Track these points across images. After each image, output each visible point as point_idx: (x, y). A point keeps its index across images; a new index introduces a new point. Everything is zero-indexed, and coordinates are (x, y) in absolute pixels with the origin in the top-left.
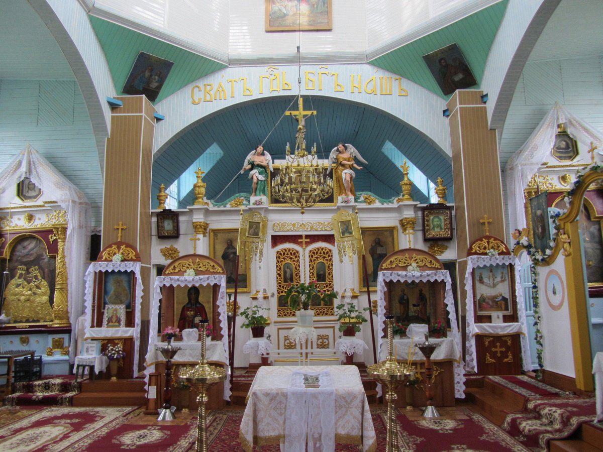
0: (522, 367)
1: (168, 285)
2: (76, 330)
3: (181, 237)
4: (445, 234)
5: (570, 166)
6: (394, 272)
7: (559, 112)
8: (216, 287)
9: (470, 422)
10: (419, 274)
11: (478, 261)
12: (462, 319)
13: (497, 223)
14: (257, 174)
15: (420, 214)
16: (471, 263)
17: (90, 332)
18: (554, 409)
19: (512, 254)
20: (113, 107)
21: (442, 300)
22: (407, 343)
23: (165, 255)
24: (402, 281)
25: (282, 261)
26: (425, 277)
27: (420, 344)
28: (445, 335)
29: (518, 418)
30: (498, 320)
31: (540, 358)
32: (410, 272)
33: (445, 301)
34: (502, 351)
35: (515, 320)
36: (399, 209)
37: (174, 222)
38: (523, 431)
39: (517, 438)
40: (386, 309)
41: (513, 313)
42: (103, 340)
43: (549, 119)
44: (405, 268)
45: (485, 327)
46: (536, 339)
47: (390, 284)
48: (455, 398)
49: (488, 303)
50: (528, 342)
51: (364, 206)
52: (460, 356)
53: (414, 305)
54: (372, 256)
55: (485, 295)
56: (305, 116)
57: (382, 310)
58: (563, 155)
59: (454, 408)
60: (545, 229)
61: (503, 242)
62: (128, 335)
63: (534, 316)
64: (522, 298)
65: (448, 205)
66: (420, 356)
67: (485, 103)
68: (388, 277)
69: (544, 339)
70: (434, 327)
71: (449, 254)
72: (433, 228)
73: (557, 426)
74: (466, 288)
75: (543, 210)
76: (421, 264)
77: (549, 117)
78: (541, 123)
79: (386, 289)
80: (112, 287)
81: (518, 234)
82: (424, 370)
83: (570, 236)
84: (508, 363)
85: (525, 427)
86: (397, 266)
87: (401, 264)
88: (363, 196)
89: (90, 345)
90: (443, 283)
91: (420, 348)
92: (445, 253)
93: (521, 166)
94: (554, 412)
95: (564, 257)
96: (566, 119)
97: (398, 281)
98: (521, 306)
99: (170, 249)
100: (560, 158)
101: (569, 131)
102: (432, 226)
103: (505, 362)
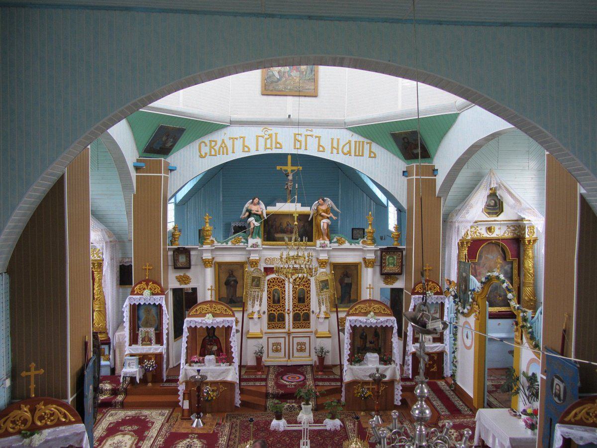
1: (193, 326)
2: (115, 341)
3: (192, 267)
5: (495, 221)
8: (229, 329)
14: (254, 222)
17: (128, 350)
20: (137, 169)
23: (179, 281)
25: (271, 287)
37: (186, 257)
42: (140, 355)
51: (336, 245)
53: (371, 343)
54: (341, 285)
56: (292, 171)
57: (348, 347)
62: (159, 351)
67: (435, 176)
72: (388, 265)
80: (142, 314)
84: (433, 372)
86: (360, 312)
87: (363, 311)
89: (131, 361)
92: (395, 283)
96: (497, 184)
97: (360, 326)
99: (183, 277)
100: (489, 213)
103: (432, 371)
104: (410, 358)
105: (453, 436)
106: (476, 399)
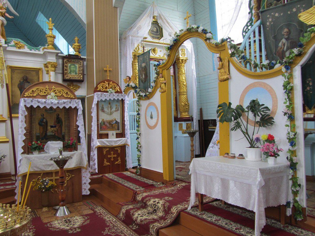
0: (126, 166)
4: (79, 77)
6: (34, 99)
7: (154, 9)
9: (94, 217)
10: (56, 102)
11: (101, 96)
12: (88, 136)
13: (115, 71)
15: (60, 61)
16: (97, 97)
18: (157, 200)
19: (123, 93)
21: (75, 122)
22: (44, 157)
24: (42, 106)
26: (61, 104)
27: (55, 158)
28: (76, 149)
29: (131, 209)
30: (112, 136)
31: (139, 160)
32: (49, 100)
33: (77, 123)
34: (114, 157)
35: (123, 136)
36: (44, 55)
38: (136, 220)
39: (131, 226)
40: (26, 130)
41: (122, 132)
43: (148, 11)
44: (45, 97)
45: (104, 141)
46: (137, 148)
47: (31, 110)
48: (83, 195)
49: (106, 126)
50: (131, 150)
52: (87, 164)
53: (52, 127)
55: (105, 120)
58: (155, 36)
59: (82, 203)
60: (147, 76)
61: (118, 85)
63: (137, 133)
64: (128, 121)
65: (82, 57)
66: (55, 167)
68: (29, 103)
69: (142, 148)
70: (68, 143)
71: (81, 92)
72: (70, 72)
73: (161, 214)
74: (92, 115)
75: (147, 64)
76: (58, 94)
77: (149, 10)
78: (144, 13)
79: (26, 113)
81: (128, 79)
82: (58, 177)
83: (166, 78)
84: (118, 164)
85: (137, 217)
86: (38, 95)
87: (42, 94)
88: (14, 42)
90: (76, 109)
91: (55, 161)
93: (131, 36)
94: (158, 203)
95: (160, 93)
96: (158, 14)
97: (38, 107)
98: (128, 127)
101: (159, 21)
102: (69, 71)
104: (96, 152)
105: (158, 204)
106: (168, 173)
